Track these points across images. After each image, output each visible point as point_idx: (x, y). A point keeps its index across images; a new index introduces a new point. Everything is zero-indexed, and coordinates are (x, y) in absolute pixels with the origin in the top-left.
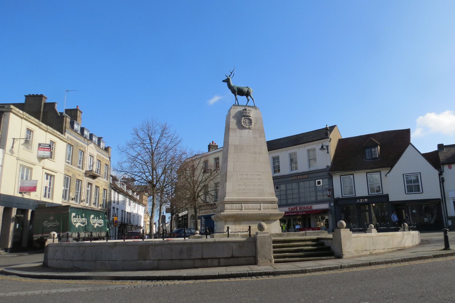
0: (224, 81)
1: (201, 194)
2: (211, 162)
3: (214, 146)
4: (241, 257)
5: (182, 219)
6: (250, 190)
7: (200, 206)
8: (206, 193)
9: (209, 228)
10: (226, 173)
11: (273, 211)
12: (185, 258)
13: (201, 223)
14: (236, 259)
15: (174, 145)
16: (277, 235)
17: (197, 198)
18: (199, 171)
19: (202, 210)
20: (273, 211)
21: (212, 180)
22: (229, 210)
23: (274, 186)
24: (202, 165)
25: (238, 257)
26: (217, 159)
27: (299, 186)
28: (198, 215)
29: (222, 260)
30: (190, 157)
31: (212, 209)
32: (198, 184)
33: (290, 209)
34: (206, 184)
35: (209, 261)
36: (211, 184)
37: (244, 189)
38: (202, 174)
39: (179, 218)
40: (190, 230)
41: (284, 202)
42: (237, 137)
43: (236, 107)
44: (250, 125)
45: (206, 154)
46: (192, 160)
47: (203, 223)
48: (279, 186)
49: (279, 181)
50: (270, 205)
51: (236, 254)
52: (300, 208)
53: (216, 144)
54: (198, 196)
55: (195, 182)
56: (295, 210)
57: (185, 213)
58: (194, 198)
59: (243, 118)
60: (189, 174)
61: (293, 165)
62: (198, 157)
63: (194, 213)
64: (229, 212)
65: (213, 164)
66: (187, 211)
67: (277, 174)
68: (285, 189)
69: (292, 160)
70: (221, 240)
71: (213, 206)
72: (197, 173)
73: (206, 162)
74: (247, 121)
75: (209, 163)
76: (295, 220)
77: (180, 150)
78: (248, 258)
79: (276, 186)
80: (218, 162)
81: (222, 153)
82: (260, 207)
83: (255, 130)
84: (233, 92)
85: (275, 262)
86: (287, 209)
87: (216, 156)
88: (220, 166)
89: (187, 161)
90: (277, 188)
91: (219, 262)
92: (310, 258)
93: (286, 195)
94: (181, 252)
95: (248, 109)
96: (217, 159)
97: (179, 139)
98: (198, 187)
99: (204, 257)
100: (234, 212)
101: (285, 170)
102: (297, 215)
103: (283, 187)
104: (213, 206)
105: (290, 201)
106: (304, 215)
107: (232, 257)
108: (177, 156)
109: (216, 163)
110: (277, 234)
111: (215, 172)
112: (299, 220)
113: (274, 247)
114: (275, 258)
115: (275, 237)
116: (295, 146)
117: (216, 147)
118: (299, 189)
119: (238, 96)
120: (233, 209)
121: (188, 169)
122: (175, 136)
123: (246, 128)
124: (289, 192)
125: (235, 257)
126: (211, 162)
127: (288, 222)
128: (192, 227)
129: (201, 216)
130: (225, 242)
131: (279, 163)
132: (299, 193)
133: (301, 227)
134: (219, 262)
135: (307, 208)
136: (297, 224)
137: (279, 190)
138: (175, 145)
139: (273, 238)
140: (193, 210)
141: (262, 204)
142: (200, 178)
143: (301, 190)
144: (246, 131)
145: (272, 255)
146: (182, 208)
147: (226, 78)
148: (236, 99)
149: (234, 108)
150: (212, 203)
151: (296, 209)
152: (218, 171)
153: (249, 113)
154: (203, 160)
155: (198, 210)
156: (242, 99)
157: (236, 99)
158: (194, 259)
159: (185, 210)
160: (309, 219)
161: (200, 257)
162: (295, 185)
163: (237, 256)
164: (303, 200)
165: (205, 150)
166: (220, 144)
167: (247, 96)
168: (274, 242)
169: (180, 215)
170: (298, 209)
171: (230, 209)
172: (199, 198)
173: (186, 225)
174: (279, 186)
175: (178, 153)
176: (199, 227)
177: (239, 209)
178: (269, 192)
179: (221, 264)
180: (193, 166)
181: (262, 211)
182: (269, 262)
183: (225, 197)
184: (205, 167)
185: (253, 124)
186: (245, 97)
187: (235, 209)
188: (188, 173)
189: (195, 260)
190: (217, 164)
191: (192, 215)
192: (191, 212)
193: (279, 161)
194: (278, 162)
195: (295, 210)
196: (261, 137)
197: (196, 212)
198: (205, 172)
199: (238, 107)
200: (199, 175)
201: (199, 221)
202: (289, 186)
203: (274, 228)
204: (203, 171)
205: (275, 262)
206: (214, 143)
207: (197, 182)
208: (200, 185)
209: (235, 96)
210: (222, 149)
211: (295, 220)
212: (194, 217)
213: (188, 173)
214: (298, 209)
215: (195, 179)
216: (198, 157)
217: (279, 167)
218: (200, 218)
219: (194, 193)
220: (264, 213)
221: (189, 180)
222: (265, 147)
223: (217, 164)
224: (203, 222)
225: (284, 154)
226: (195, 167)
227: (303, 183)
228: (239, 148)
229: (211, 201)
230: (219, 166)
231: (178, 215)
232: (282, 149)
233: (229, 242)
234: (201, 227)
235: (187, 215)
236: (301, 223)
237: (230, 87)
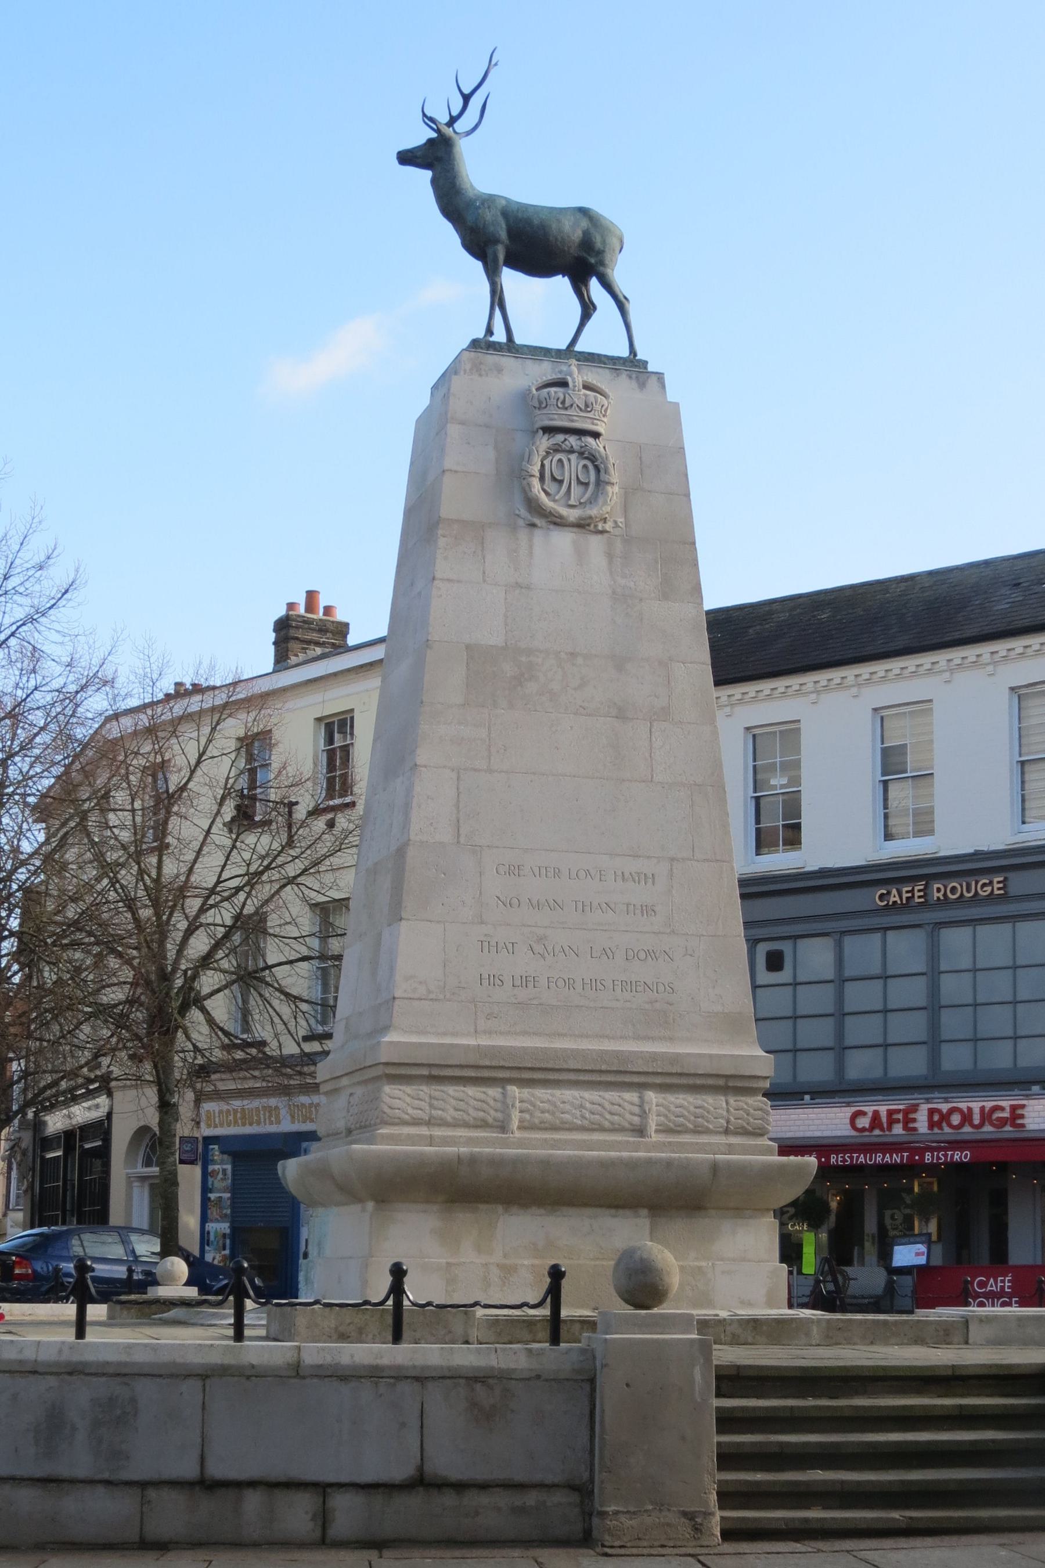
0: (406, 158)
1: (208, 981)
2: (297, 749)
3: (322, 628)
4: (484, 1486)
5: (69, 1149)
6: (570, 983)
7: (203, 1071)
8: (249, 978)
9: (261, 1260)
10: (401, 853)
11: (731, 1149)
12: (81, 1473)
13: (205, 1189)
14: (449, 1499)
15: (20, 614)
16: (757, 1329)
17: (184, 1009)
18: (198, 820)
19: (218, 1095)
20: (731, 1149)
21: (291, 881)
22: (418, 1128)
23: (753, 943)
24: (222, 768)
25: (460, 1487)
26: (337, 727)
27: (934, 954)
28: (183, 1129)
29: (342, 1503)
30: (134, 702)
31: (285, 1091)
32: (193, 905)
33: (863, 1122)
34: (249, 909)
35: (253, 1501)
36: (292, 917)
37: (526, 981)
38: (221, 837)
39: (45, 1143)
40: (125, 1242)
41: (817, 1069)
42: (488, 591)
43: (492, 359)
44: (592, 501)
45: (264, 686)
46: (151, 731)
47: (221, 1194)
48: (786, 947)
49: (784, 911)
50: (714, 1104)
51: (446, 1463)
52: (938, 1119)
53: (340, 616)
54: (191, 999)
55: (166, 897)
56: (898, 1129)
57: (82, 1113)
58: (164, 1004)
59: (544, 443)
60: (125, 836)
61: (901, 794)
62: (195, 704)
63: (153, 1119)
64: (411, 1140)
65: (307, 769)
66: (103, 1100)
67: (780, 861)
68: (829, 974)
69: (892, 762)
70: (345, 1360)
71: (294, 1074)
72: (187, 828)
73: (255, 747)
74: (574, 465)
75: (276, 761)
76: (888, 1200)
77: (62, 654)
78: (531, 1498)
79: (762, 949)
80: (346, 750)
81: (373, 683)
82: (644, 1114)
83: (627, 540)
84: (478, 243)
85: (728, 1535)
86: (830, 1121)
87: (333, 701)
88: (361, 786)
89: (114, 731)
90: (775, 962)
91: (324, 1518)
92: (984, 1513)
93: (840, 1015)
94: (53, 1427)
95: (578, 375)
96: (337, 727)
97: (58, 575)
98: (189, 932)
99: (217, 1470)
100: (446, 1141)
101: (841, 833)
102: (911, 1169)
103: (815, 957)
104: (294, 1074)
105: (861, 1066)
106: (960, 1165)
107: (421, 1482)
108: (41, 698)
109: (331, 754)
110: (755, 1324)
111: (319, 824)
112: (924, 1206)
113: (726, 1421)
114: (728, 1497)
115: (735, 1341)
116: (926, 660)
117: (332, 635)
118: (933, 974)
119: (511, 279)
120: (443, 1123)
121: (120, 797)
122: (32, 554)
123: (557, 522)
124: (859, 996)
125: (442, 1485)
126: (297, 749)
127: (840, 1214)
128: (141, 1216)
129: (208, 1140)
130: (374, 1374)
131: (796, 780)
132: (934, 1007)
133: (937, 1261)
134: (324, 1518)
135: (986, 1116)
136: (908, 1235)
137: (784, 976)
138: (30, 620)
139: (728, 1355)
140: (151, 1095)
141: (651, 1095)
142: (205, 876)
143: (952, 988)
144: (563, 540)
145: (710, 1481)
146: (73, 1074)
147: (421, 135)
148: (498, 299)
149: (477, 368)
150: (291, 1048)
151: (908, 1121)
152: (342, 821)
153: (587, 407)
154: (234, 727)
155: (185, 1101)
156: (541, 306)
157: (498, 299)
158: (143, 1485)
159: (90, 1094)
160: (999, 1201)
161: (189, 1470)
162: (906, 949)
163: (454, 1475)
164: (956, 1059)
165: (255, 657)
166: (367, 617)
167: (579, 285)
168: (731, 1381)
169: (56, 1122)
170: (922, 1123)
171: (416, 1122)
172: (195, 1015)
173: (92, 1208)
174: (786, 947)
175: (55, 676)
176: (189, 1221)
177: (484, 1125)
178: (707, 1002)
179: (342, 1525)
180: (159, 769)
181: (655, 1149)
182: (684, 1529)
183: (386, 1029)
184: (243, 783)
185: (613, 491)
186: (561, 284)
187: (455, 1125)
188: (121, 823)
189: (152, 1493)
190: (337, 761)
191: (143, 1131)
192: (132, 1110)
193: (797, 765)
194: (793, 767)
195: (898, 1129)
196: (667, 591)
197: (166, 1107)
198: (245, 818)
199: (507, 361)
200: (202, 847)
201: (189, 1177)
202: (864, 951)
203: (737, 1276)
204: (229, 812)
205: (728, 1535)
206: (323, 602)
207: (182, 892)
208: (209, 917)
209: (492, 274)
210: (378, 653)
211: (888, 1200)
212: (154, 1144)
213: (121, 823)
214: (922, 1123)
215: (170, 868)
216: (195, 704)
217: (792, 805)
218: (199, 1152)
219: (165, 977)
220: (669, 1164)
221: (127, 877)
222: (697, 654)
223: (337, 761)
224: (217, 1182)
225: (833, 715)
226: (174, 781)
227: (966, 932)
228: (502, 674)
229: (286, 1039)
230: (346, 787)
231: (38, 1125)
232: (822, 677)
233: (399, 1376)
234: (204, 1219)
235: (102, 1129)
236: (933, 1227)
237: (452, 201)
